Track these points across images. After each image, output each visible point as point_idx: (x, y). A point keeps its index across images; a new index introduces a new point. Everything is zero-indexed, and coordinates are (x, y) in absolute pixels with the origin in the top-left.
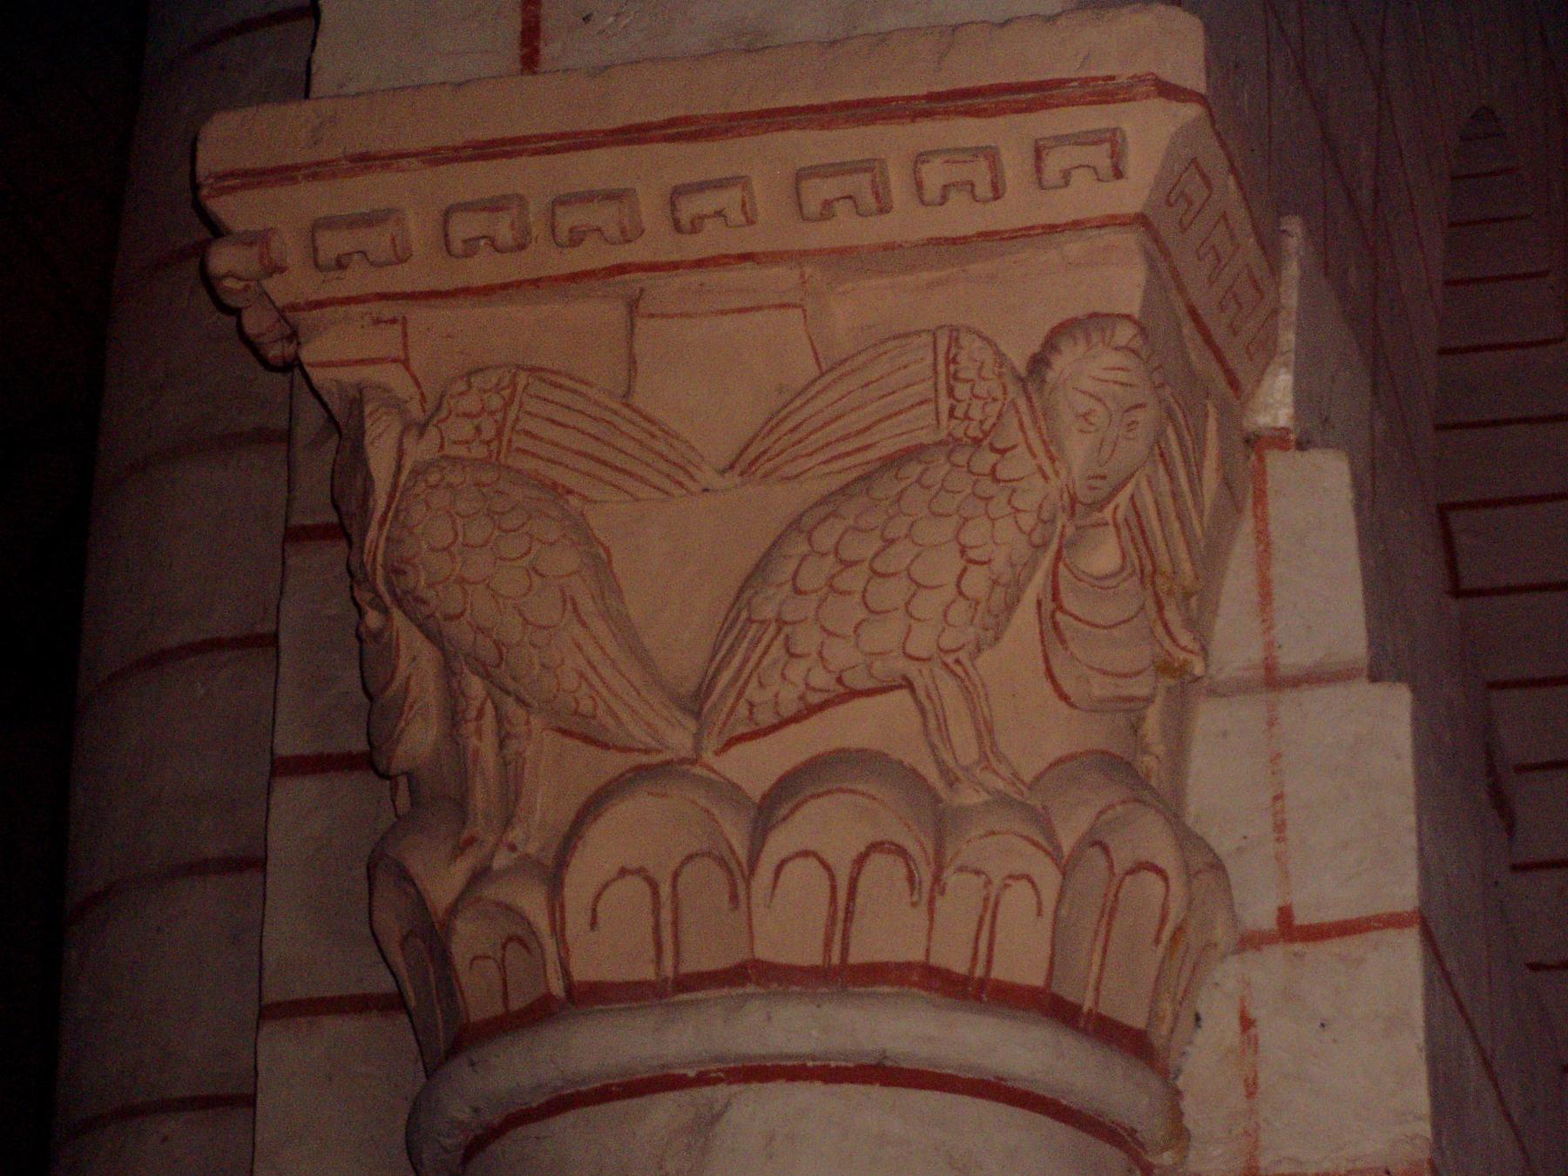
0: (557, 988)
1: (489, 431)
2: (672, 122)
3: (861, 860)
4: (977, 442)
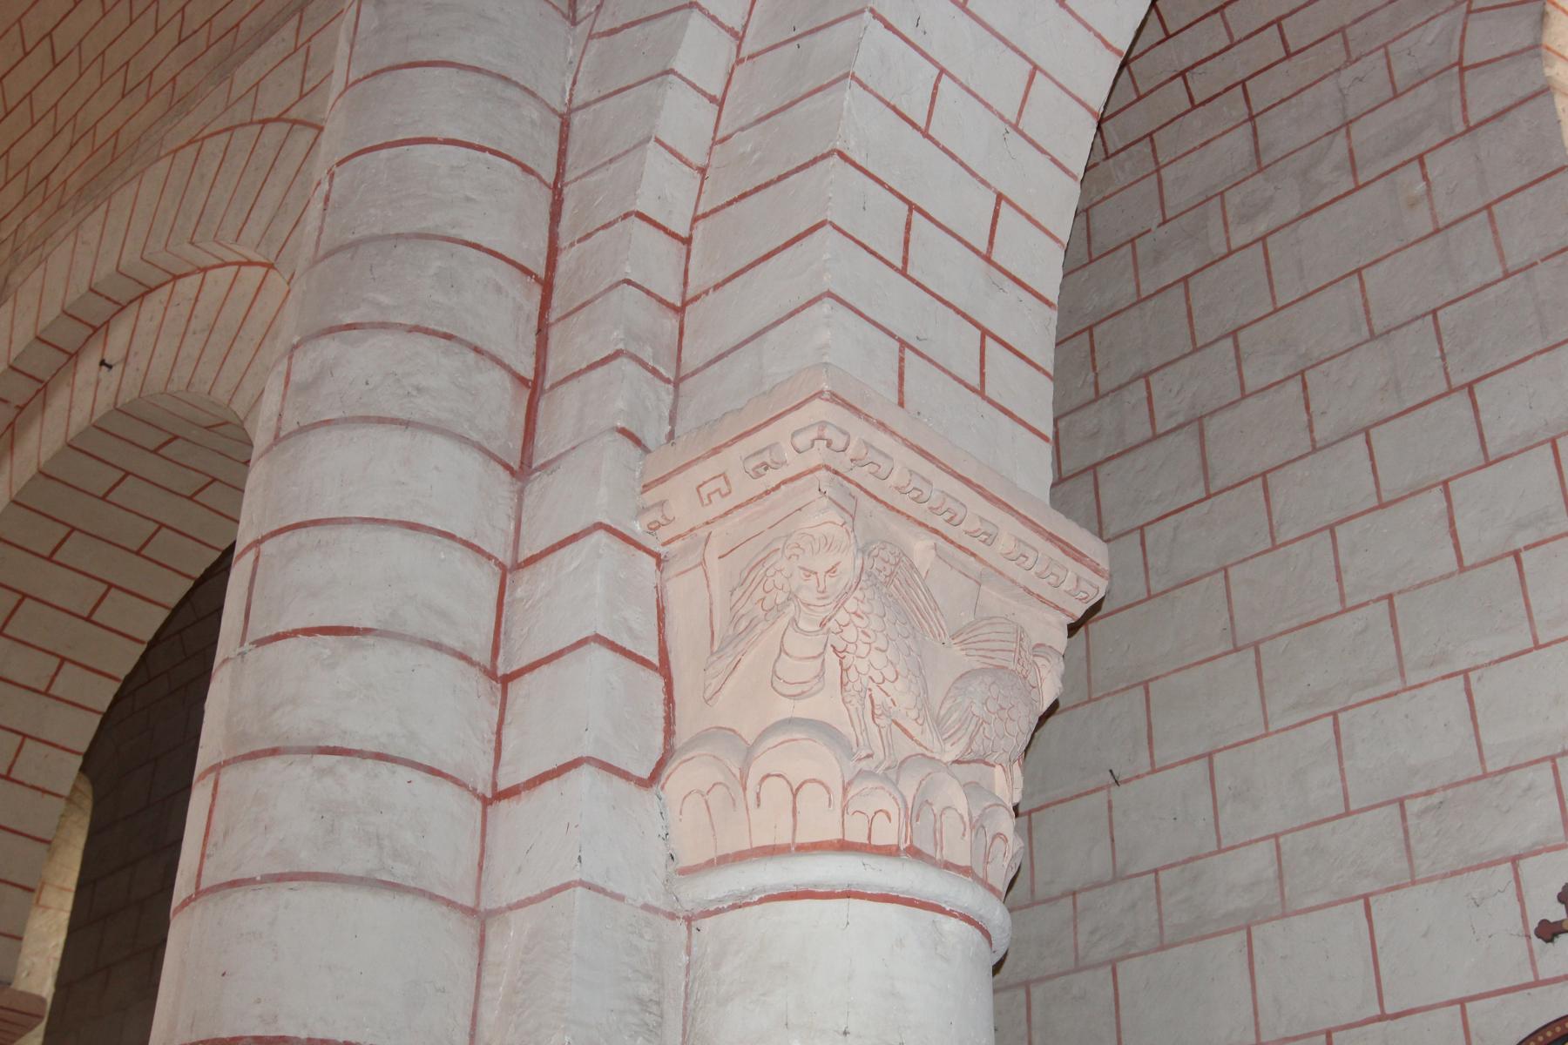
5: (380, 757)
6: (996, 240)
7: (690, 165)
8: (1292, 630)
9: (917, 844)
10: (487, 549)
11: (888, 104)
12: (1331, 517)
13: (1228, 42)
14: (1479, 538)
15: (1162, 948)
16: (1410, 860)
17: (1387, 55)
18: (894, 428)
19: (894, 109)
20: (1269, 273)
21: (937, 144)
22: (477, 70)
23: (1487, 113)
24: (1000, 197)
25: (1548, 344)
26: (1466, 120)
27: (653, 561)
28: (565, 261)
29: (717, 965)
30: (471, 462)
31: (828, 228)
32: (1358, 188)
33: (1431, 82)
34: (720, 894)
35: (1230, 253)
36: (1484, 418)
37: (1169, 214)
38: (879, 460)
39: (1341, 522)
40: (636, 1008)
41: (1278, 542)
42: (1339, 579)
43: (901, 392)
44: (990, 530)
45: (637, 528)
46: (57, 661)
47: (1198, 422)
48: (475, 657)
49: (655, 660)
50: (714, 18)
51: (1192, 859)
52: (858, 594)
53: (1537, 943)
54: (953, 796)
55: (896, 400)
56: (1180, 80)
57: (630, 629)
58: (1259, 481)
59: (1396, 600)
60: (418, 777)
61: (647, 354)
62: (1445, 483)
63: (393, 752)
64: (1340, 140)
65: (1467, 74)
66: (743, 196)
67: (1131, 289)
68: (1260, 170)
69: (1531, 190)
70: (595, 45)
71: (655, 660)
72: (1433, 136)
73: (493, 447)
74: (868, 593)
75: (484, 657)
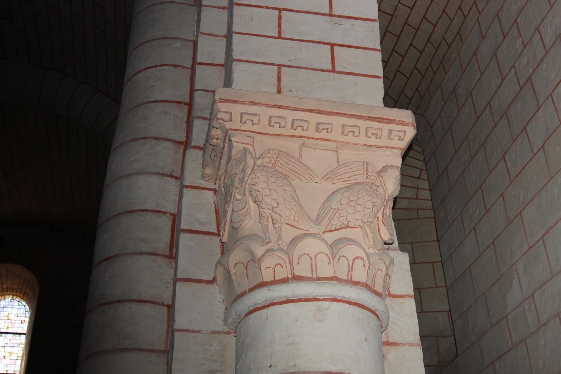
0: (290, 276)
1: (273, 161)
2: (317, 110)
3: (354, 260)
4: (372, 184)
7: (219, 37)
27: (212, 193)
55: (275, 90)
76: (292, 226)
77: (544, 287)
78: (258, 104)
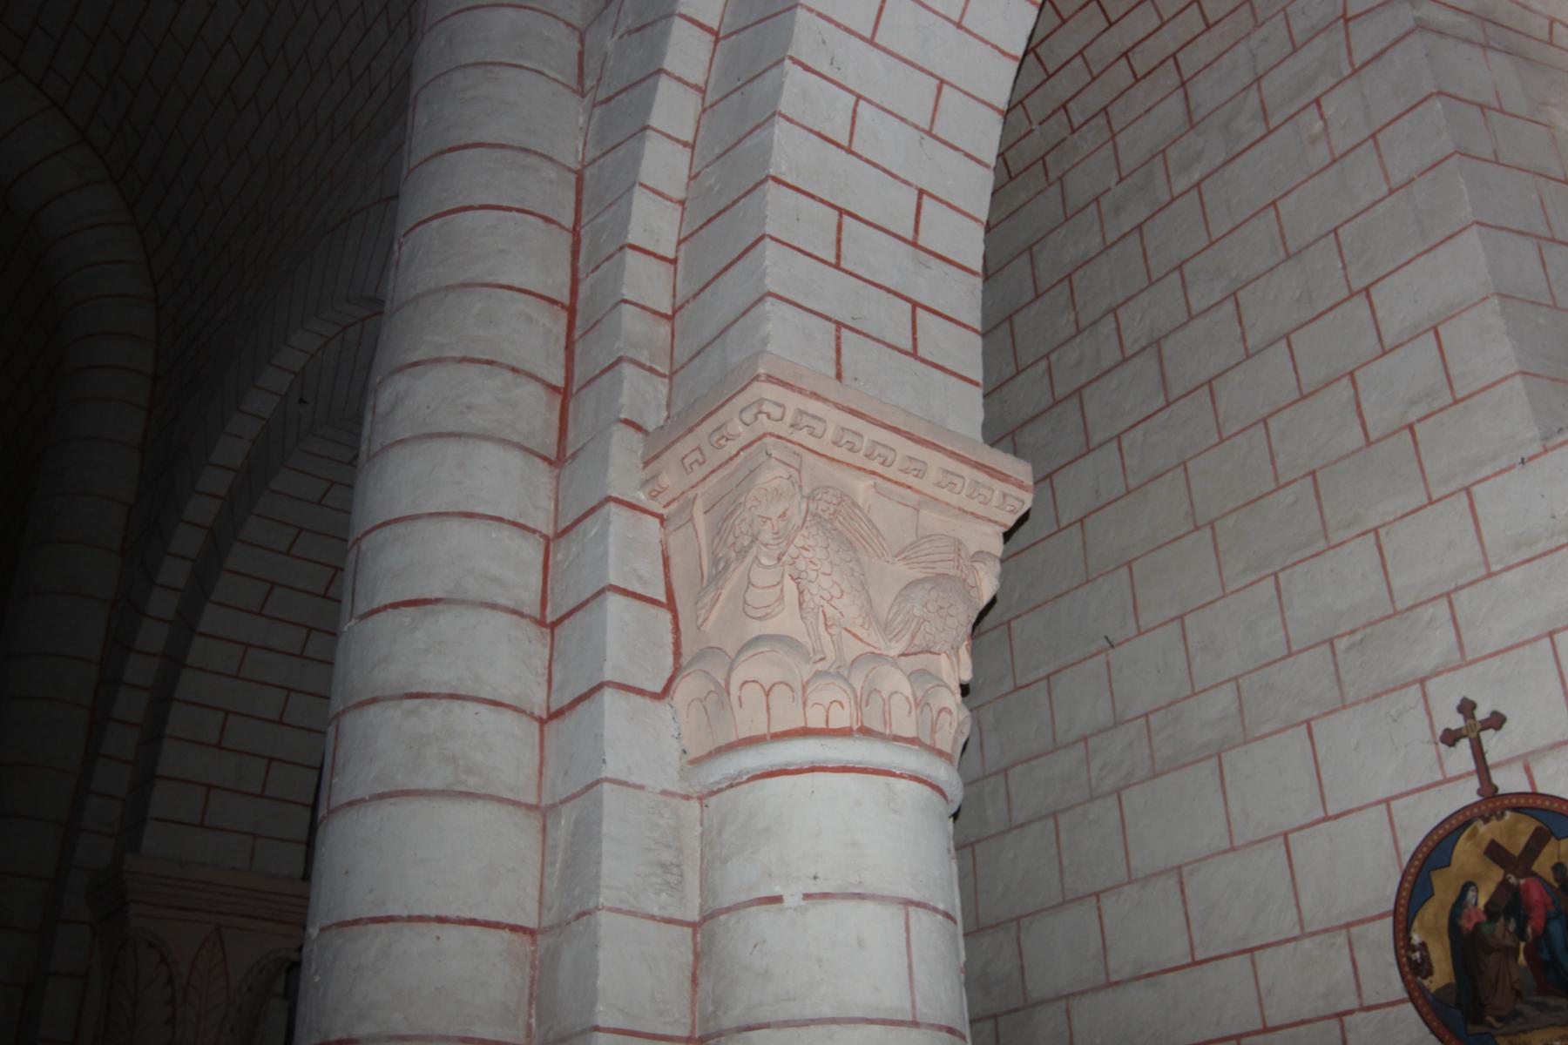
1: (832, 509)
5: (453, 696)
6: (921, 228)
7: (671, 200)
8: (1238, 508)
9: (867, 724)
10: (531, 524)
11: (812, 131)
12: (1265, 411)
13: (1158, 23)
14: (1381, 417)
15: (1155, 776)
16: (1340, 687)
17: (1286, 17)
18: (826, 395)
19: (819, 135)
20: (1204, 213)
21: (860, 157)
22: (503, 146)
23: (1368, 56)
24: (921, 192)
25: (1426, 246)
26: (1352, 64)
27: (656, 521)
28: (583, 290)
29: (720, 833)
30: (515, 459)
31: (767, 240)
32: (1270, 132)
33: (1323, 35)
34: (717, 778)
35: (1174, 199)
36: (1380, 315)
37: (1124, 173)
38: (813, 423)
39: (1271, 415)
40: (659, 871)
41: (1225, 435)
42: (1273, 463)
43: (838, 363)
44: (919, 466)
45: (641, 497)
46: (305, 631)
47: (1156, 344)
48: (526, 611)
49: (663, 599)
50: (679, 79)
51: (1172, 703)
52: (804, 532)
53: (1443, 747)
54: (896, 683)
55: (832, 372)
56: (1123, 61)
57: (640, 578)
58: (1206, 388)
59: (1319, 475)
60: (482, 708)
61: (644, 357)
62: (1351, 374)
63: (462, 692)
64: (1253, 95)
65: (1350, 24)
66: (710, 220)
67: (1098, 240)
68: (1193, 126)
69: (1406, 117)
70: (598, 111)
71: (663, 599)
72: (1326, 81)
73: (531, 445)
74: (813, 530)
75: (535, 611)
76: (855, 635)
77: (1034, 763)
78: (825, 400)
